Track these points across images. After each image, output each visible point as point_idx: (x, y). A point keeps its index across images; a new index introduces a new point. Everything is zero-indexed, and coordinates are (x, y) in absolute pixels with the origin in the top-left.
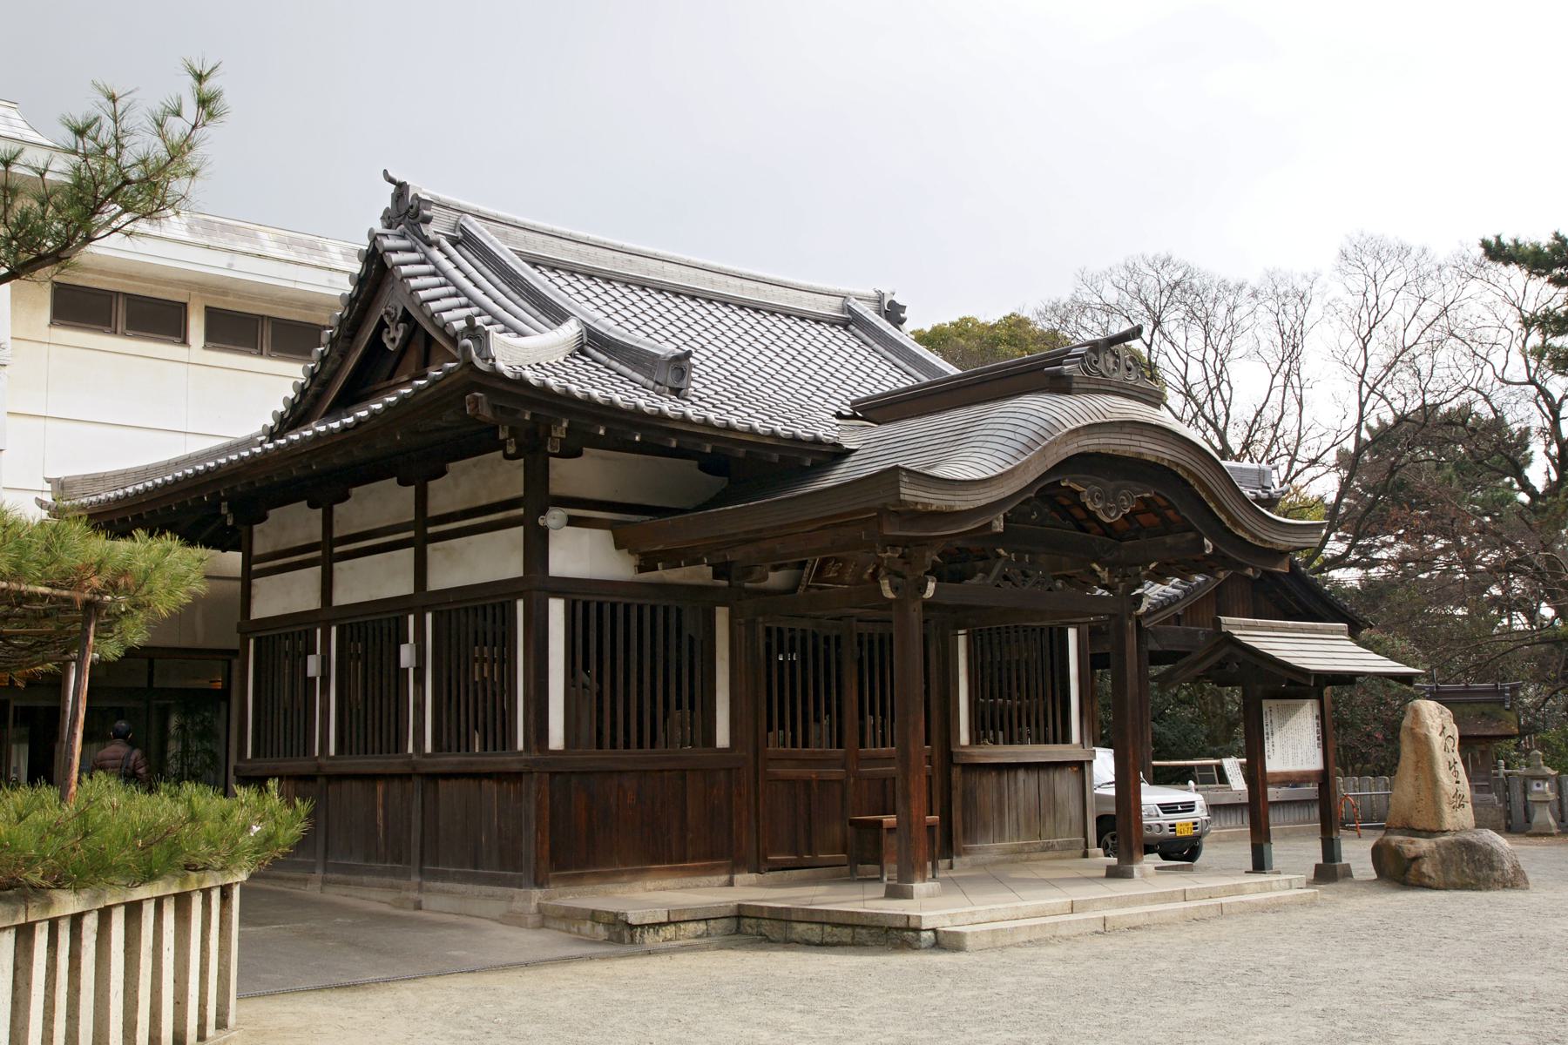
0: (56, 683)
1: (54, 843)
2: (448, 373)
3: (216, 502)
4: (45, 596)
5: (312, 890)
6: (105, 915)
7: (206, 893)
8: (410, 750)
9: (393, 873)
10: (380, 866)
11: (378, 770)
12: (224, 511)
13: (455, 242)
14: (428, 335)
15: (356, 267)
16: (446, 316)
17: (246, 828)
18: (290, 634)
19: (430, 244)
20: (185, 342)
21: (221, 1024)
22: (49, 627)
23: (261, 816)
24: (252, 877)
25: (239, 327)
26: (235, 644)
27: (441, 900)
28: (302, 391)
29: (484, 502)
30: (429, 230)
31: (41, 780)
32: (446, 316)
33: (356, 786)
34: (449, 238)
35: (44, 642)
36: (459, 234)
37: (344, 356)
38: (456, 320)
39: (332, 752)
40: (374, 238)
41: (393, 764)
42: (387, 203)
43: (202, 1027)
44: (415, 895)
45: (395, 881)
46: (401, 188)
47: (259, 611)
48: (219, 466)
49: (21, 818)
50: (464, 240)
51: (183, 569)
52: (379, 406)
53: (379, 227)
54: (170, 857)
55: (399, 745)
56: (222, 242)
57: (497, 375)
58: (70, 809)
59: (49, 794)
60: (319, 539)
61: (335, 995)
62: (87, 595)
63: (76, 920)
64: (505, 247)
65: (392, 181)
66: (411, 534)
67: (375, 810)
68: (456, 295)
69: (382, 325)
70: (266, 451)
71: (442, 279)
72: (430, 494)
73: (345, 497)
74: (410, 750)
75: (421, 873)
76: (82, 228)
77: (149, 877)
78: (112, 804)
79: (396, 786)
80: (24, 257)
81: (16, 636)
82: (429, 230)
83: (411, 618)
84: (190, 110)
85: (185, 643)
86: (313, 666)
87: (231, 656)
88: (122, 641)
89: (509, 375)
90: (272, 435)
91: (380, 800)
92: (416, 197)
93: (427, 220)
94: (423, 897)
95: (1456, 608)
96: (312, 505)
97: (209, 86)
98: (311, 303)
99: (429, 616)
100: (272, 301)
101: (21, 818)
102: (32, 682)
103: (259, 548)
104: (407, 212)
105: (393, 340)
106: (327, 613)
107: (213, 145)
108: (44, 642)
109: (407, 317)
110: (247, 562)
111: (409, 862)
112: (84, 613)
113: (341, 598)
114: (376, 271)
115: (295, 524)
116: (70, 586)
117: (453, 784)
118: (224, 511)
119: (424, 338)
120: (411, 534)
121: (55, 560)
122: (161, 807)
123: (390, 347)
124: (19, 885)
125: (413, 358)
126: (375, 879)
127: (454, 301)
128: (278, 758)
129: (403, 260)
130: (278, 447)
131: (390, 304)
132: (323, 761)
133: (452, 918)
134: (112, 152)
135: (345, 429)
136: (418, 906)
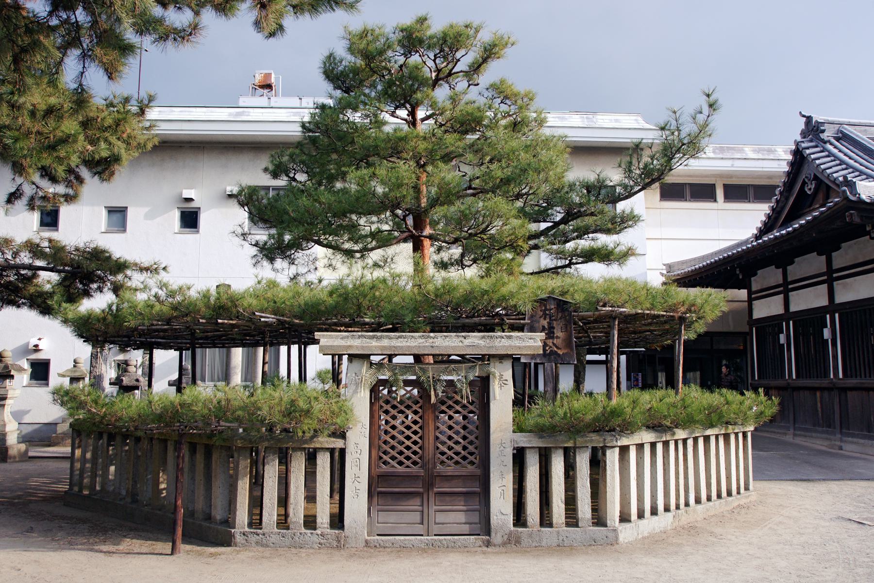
0: (672, 347)
1: (672, 411)
2: (836, 204)
3: (733, 269)
4: (663, 316)
5: (789, 438)
6: (696, 440)
7: (736, 434)
8: (832, 377)
9: (827, 433)
10: (820, 429)
11: (816, 385)
12: (738, 272)
13: (838, 139)
14: (827, 186)
15: (790, 157)
16: (835, 175)
17: (751, 408)
18: (772, 324)
19: (825, 142)
20: (715, 201)
21: (747, 488)
22: (667, 327)
23: (756, 404)
24: (756, 429)
25: (739, 191)
26: (747, 329)
27: (851, 447)
28: (769, 217)
29: (861, 261)
30: (824, 136)
31: (669, 387)
32: (835, 175)
33: (807, 393)
34: (835, 138)
35: (666, 332)
36: (840, 135)
37: (787, 199)
38: (839, 176)
39: (794, 377)
40: (797, 144)
41: (824, 383)
42: (803, 127)
43: (738, 488)
44: (838, 443)
45: (829, 437)
46: (809, 119)
47: (756, 315)
48: (733, 254)
49: (661, 400)
50: (843, 137)
51: (717, 301)
52: (803, 222)
53: (799, 138)
54: (719, 419)
55: (826, 374)
56: (728, 155)
57: (861, 202)
58: (678, 398)
59: (671, 392)
60: (781, 282)
61: (799, 483)
62: (680, 314)
63: (685, 441)
64: (864, 137)
65: (804, 116)
66: (826, 277)
67: (816, 404)
68: (840, 165)
69: (804, 183)
70: (753, 246)
71: (832, 158)
72: (833, 259)
73: (792, 263)
74: (832, 377)
75: (841, 433)
76: (668, 167)
77: (712, 426)
78: (695, 396)
79: (826, 394)
80: (647, 181)
81: (655, 331)
82: (824, 136)
83: (828, 316)
84: (706, 110)
85: (725, 330)
86: (782, 339)
87: (745, 336)
88: (696, 332)
89: (868, 201)
90: (757, 238)
91: (818, 399)
92: (817, 122)
93: (823, 131)
94: (842, 444)
95: (727, 366)
96: (777, 267)
97: (712, 98)
98: (770, 176)
99: (837, 315)
100: (753, 178)
101: (661, 400)
102: (663, 347)
103: (754, 289)
104: (812, 129)
105: (810, 189)
106: (788, 315)
107: (717, 122)
108: (666, 332)
109: (816, 178)
110: (750, 293)
111: (835, 428)
112: (674, 323)
113: (793, 308)
114: (799, 159)
115: (770, 276)
116: (673, 311)
117: (854, 393)
118: (738, 272)
119: (825, 187)
120: (826, 277)
121: (666, 302)
122: (714, 398)
123: (809, 193)
124: (662, 426)
125: (820, 196)
126: (819, 435)
127: (839, 167)
128: (769, 379)
129: (812, 152)
130: (758, 244)
131: (806, 172)
132: (790, 381)
133: (859, 455)
134: (676, 133)
135: (788, 233)
136: (841, 448)
